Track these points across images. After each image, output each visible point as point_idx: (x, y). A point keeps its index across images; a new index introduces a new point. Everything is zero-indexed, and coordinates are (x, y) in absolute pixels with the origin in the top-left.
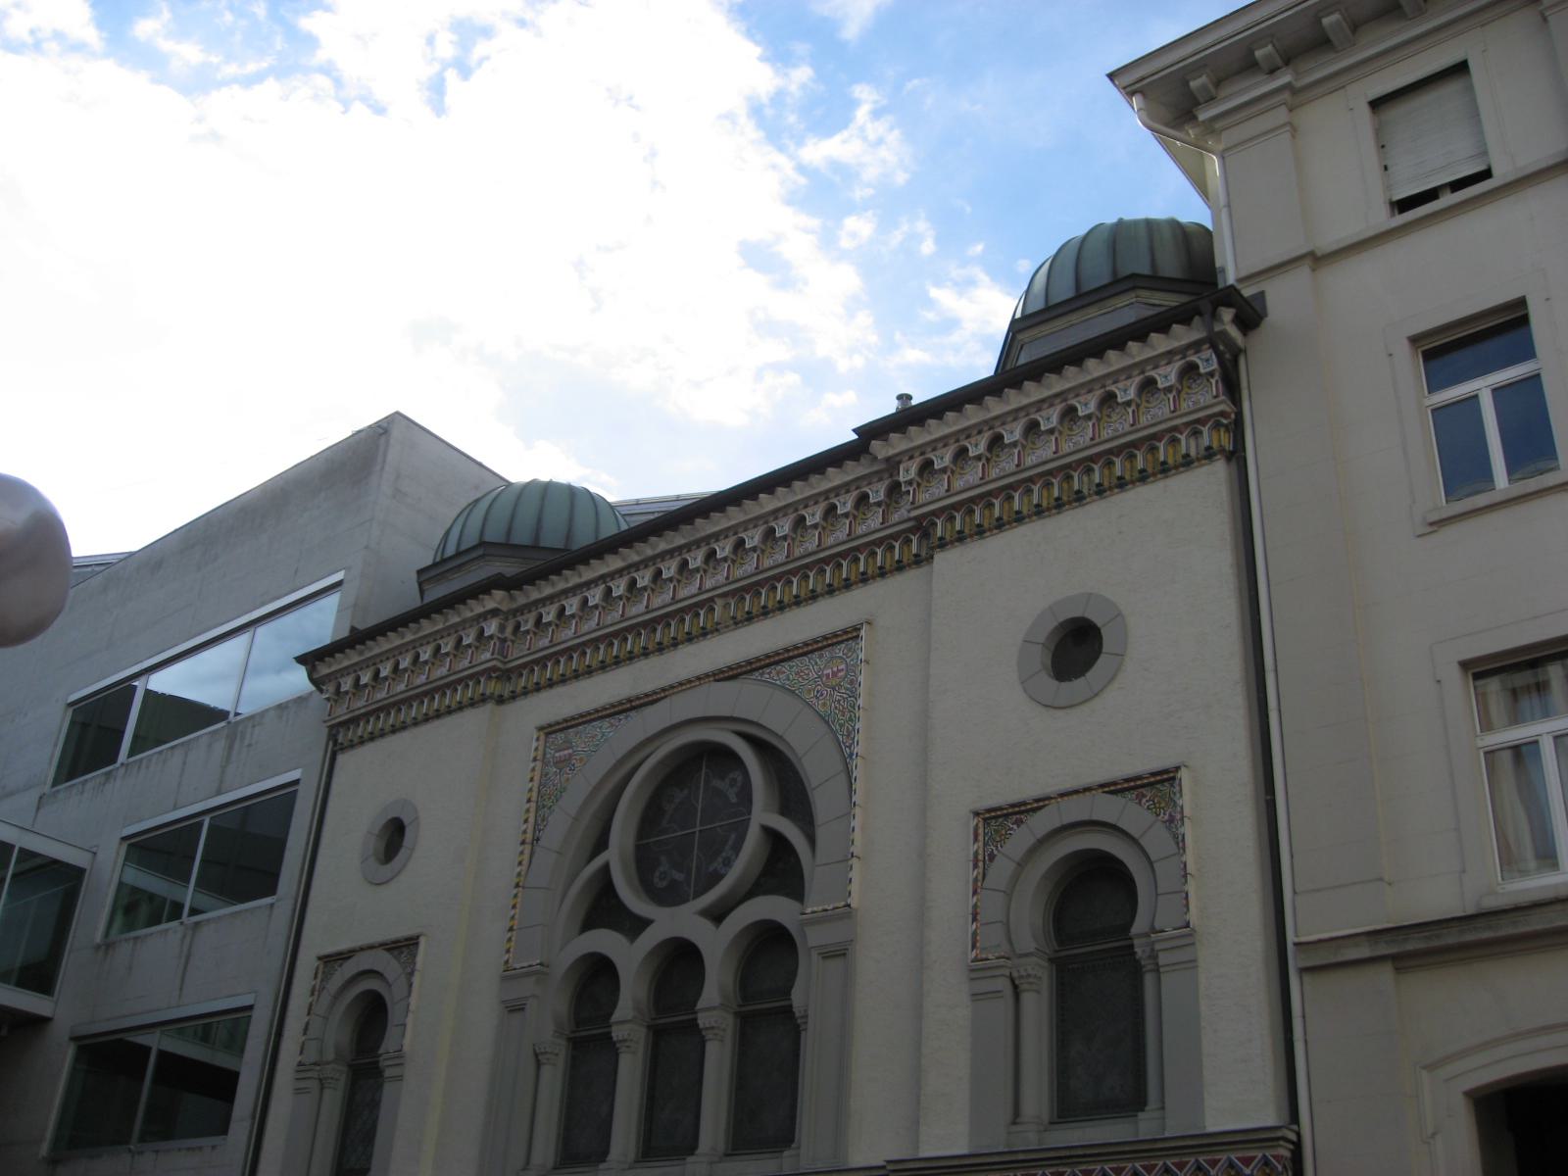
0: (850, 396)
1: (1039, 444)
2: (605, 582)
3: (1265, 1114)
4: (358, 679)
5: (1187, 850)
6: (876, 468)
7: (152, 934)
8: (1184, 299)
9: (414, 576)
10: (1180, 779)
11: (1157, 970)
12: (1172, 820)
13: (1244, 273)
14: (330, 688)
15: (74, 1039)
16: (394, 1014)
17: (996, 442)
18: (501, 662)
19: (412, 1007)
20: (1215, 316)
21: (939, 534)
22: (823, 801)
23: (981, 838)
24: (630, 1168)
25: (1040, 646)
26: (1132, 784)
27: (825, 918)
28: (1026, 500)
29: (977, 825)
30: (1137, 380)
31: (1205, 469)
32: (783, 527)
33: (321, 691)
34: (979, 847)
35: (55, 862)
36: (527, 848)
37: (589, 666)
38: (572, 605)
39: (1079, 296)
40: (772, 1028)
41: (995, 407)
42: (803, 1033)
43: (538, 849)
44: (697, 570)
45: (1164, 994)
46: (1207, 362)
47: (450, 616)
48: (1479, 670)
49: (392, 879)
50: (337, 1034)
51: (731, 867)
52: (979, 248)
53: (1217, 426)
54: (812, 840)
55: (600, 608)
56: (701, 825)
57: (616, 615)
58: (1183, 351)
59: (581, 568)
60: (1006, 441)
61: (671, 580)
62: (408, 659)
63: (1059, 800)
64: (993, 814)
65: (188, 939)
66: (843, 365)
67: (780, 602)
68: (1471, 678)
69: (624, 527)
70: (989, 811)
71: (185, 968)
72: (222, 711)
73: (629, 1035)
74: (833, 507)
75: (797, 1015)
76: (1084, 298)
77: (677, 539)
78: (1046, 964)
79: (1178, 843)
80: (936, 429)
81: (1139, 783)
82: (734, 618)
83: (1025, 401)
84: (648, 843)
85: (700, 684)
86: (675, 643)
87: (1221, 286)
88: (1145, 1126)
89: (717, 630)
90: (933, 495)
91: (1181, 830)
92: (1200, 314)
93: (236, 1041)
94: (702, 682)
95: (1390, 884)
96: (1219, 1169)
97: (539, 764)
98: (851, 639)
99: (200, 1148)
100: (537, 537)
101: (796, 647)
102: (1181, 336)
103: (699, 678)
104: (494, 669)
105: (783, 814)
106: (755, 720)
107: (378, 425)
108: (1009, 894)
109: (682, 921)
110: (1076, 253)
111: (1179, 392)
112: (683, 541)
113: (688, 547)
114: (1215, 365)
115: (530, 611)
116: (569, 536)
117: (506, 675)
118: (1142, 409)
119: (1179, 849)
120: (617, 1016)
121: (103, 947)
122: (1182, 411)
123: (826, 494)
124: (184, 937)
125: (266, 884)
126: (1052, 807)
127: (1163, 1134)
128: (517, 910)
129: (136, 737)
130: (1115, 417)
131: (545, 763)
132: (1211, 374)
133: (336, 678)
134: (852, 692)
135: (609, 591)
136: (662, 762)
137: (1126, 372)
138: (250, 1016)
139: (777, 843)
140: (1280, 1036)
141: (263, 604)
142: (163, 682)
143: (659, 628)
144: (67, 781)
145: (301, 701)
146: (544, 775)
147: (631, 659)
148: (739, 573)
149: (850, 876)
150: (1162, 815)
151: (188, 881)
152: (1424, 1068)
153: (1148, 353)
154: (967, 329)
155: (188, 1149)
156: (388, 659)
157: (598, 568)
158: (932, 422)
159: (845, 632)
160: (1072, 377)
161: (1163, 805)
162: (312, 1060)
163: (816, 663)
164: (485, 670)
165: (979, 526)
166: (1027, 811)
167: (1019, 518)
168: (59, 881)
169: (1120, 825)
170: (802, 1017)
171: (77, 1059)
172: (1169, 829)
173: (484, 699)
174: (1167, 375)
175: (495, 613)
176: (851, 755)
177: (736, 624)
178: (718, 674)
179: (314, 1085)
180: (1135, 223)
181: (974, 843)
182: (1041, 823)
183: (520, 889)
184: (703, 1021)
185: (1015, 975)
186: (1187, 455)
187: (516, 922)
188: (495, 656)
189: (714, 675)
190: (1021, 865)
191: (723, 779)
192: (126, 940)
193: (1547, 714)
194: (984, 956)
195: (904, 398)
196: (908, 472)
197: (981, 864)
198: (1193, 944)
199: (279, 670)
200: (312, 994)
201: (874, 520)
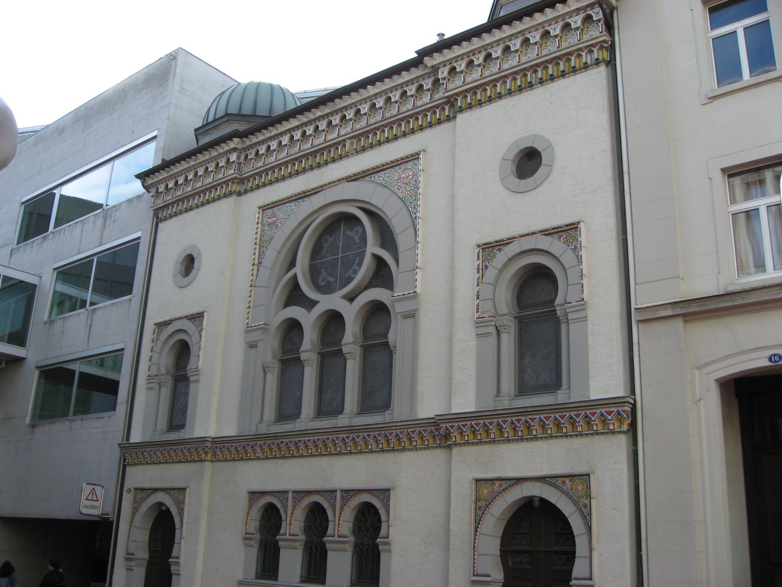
2: (290, 133)
3: (619, 391)
6: (427, 71)
22: (403, 241)
23: (481, 258)
36: (256, 267)
45: (571, 334)
85: (340, 183)
88: (561, 397)
89: (347, 156)
94: (340, 182)
103: (339, 180)
117: (242, 181)
127: (557, 402)
139: (380, 262)
159: (412, 156)
163: (398, 172)
177: (357, 152)
179: (156, 386)
197: (481, 271)
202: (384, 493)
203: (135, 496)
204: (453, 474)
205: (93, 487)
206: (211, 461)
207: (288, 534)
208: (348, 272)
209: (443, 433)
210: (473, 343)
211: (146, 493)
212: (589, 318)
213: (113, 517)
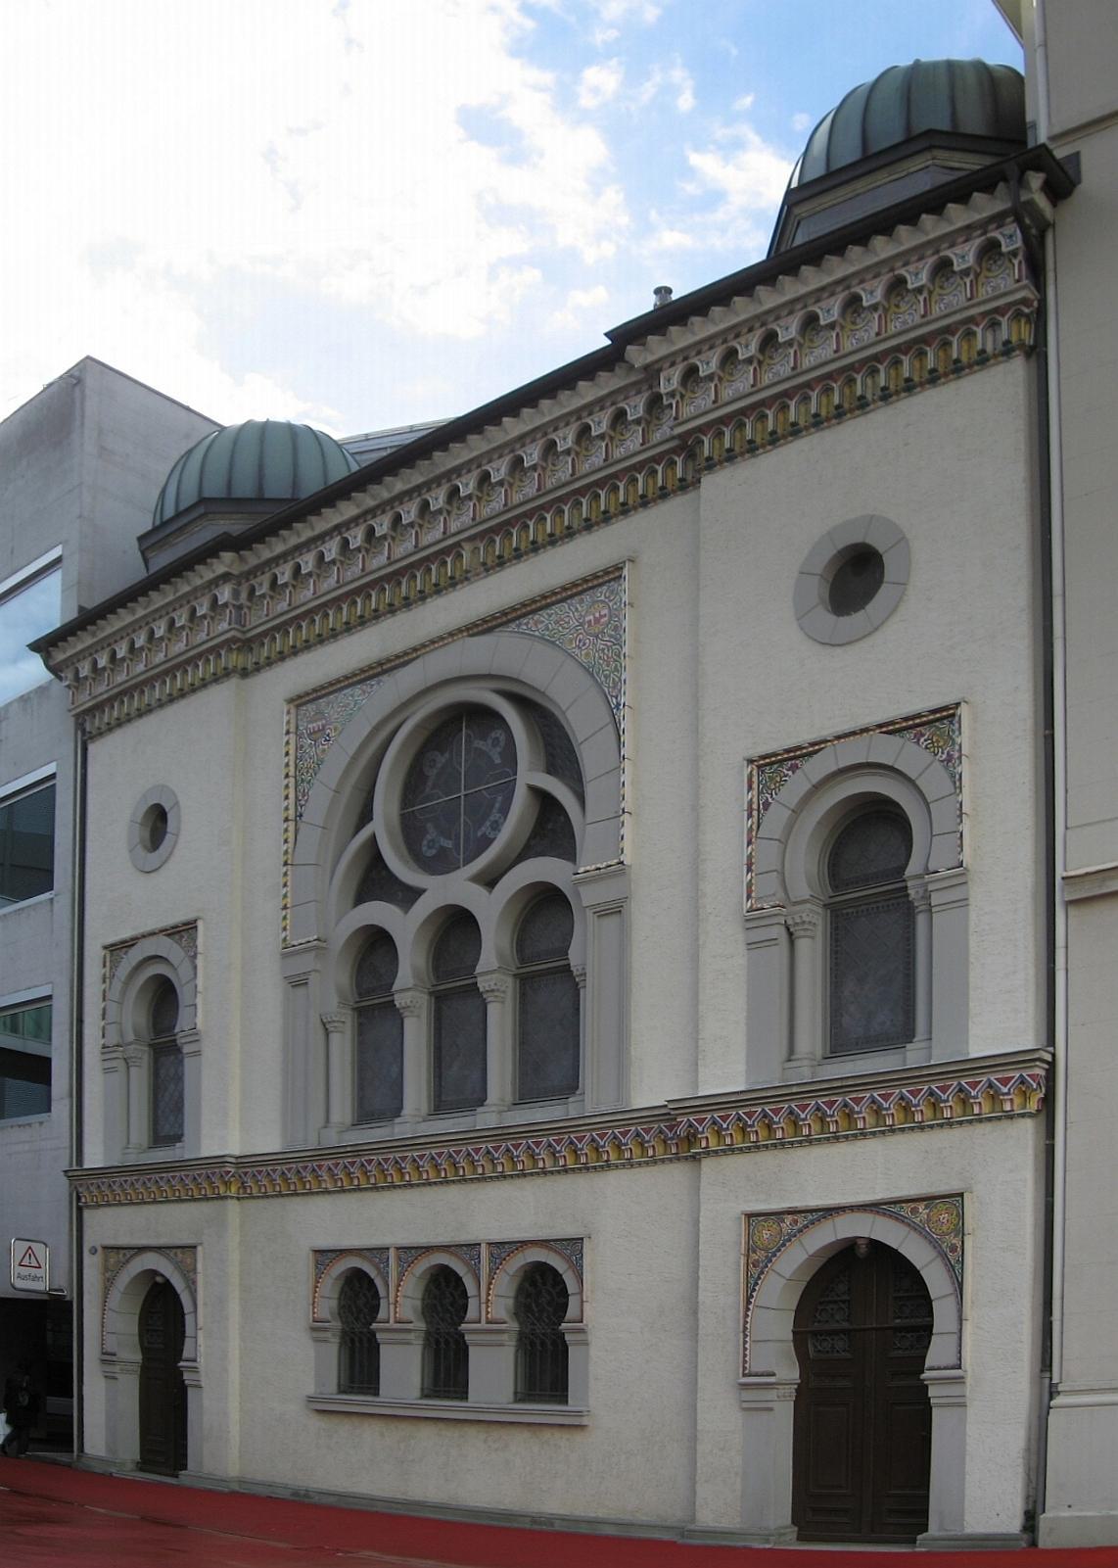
0: (600, 293)
1: (818, 341)
3: (1025, 1038)
4: (95, 662)
6: (633, 379)
8: (988, 161)
9: (135, 543)
12: (950, 758)
13: (1057, 130)
14: (69, 674)
16: (184, 995)
17: (769, 341)
20: (1021, 182)
21: (706, 453)
22: (591, 758)
27: (600, 876)
28: (803, 409)
30: (931, 261)
31: (1000, 368)
32: (532, 455)
33: (60, 678)
36: (291, 826)
38: (308, 562)
39: (866, 158)
41: (768, 298)
43: (302, 826)
44: (440, 511)
45: (936, 934)
46: (1010, 239)
50: (133, 1017)
52: (748, 100)
53: (1018, 315)
54: (581, 797)
57: (357, 570)
58: (983, 226)
59: (313, 519)
60: (781, 340)
61: (411, 525)
66: (590, 256)
67: (534, 542)
69: (355, 468)
70: (763, 757)
74: (586, 429)
76: (872, 161)
77: (413, 477)
80: (700, 329)
82: (484, 564)
83: (803, 290)
86: (423, 597)
87: (1031, 145)
88: (913, 1056)
90: (699, 406)
92: (1005, 180)
93: (43, 1030)
97: (292, 736)
100: (260, 487)
101: (554, 593)
102: (985, 206)
103: (451, 634)
104: (234, 640)
105: (549, 773)
107: (69, 374)
108: (784, 842)
110: (863, 105)
111: (977, 275)
112: (421, 480)
113: (428, 485)
114: (1019, 243)
116: (295, 484)
117: (247, 645)
118: (935, 297)
122: (981, 298)
123: (577, 413)
125: (42, 880)
126: (141, 944)
130: (904, 307)
131: (299, 736)
132: (1014, 254)
135: (346, 542)
136: (418, 727)
137: (919, 252)
139: (545, 801)
145: (42, 691)
147: (377, 618)
148: (486, 512)
153: (945, 228)
154: (733, 203)
157: (331, 517)
158: (696, 320)
159: (606, 572)
160: (857, 259)
165: (750, 442)
167: (795, 431)
172: (946, 768)
173: (227, 673)
174: (964, 255)
175: (226, 577)
179: (120, 1065)
180: (935, 65)
182: (817, 768)
186: (983, 351)
190: (796, 812)
191: (484, 738)
195: (663, 292)
196: (670, 381)
201: (633, 441)
202: (572, 1247)
203: (106, 1261)
209: (682, 1134)
212: (971, 900)
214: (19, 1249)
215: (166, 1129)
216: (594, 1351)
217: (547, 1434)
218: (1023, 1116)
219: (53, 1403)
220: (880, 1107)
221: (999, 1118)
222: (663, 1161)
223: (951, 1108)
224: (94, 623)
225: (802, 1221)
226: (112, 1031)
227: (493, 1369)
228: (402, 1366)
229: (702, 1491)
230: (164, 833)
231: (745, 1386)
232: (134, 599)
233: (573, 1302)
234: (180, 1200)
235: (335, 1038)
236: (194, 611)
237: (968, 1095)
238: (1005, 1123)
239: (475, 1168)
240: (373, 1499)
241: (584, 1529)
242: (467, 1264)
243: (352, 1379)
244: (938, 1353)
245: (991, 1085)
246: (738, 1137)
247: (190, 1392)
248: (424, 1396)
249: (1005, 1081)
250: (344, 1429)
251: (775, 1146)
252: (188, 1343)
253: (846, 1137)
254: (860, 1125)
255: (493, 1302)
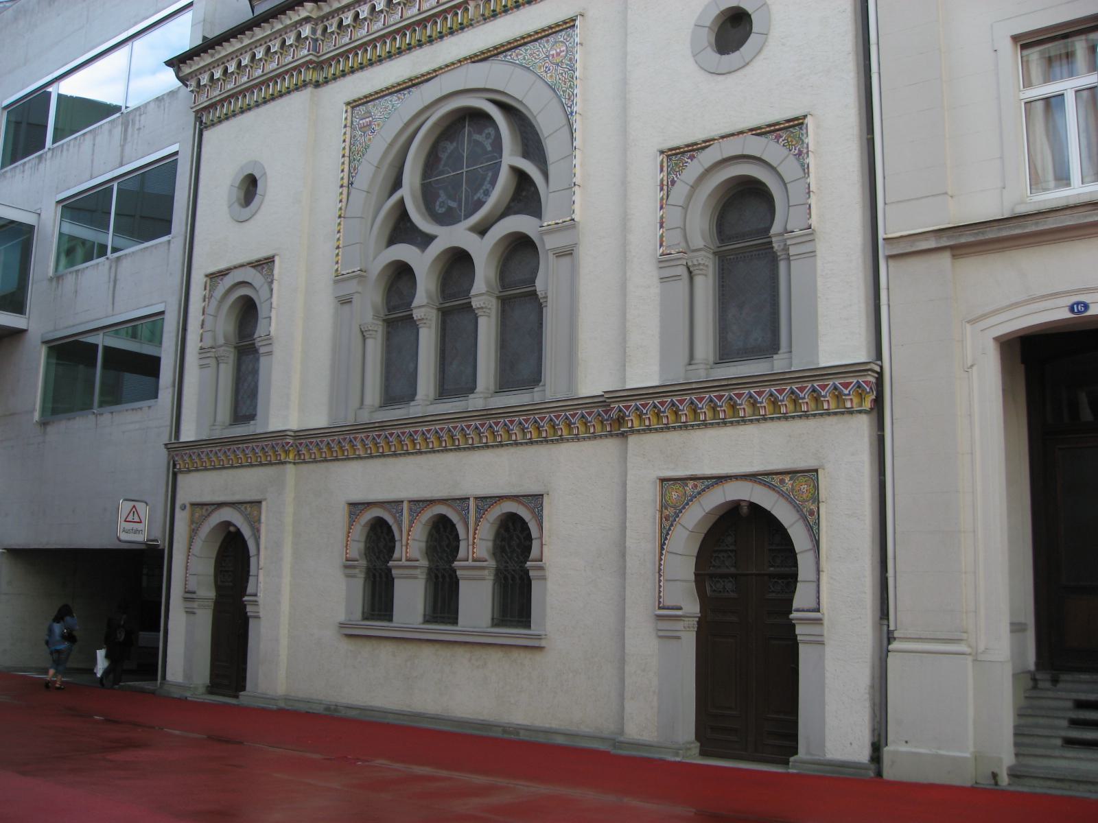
3: (859, 353)
4: (212, 75)
5: (810, 175)
7: (87, 268)
10: (807, 125)
11: (788, 259)
12: (800, 153)
15: (44, 342)
16: (262, 311)
18: (314, 55)
19: (274, 305)
22: (553, 149)
23: (665, 169)
24: (431, 404)
25: (707, 29)
26: (772, 128)
27: (558, 229)
29: (662, 160)
33: (187, 86)
34: (664, 176)
35: (12, 222)
36: (345, 190)
37: (379, 56)
40: (522, 303)
42: (544, 309)
43: (353, 191)
45: (793, 276)
47: (275, 24)
48: (1025, 42)
49: (251, 218)
50: (225, 326)
51: (489, 196)
54: (546, 175)
55: (385, 13)
56: (466, 168)
62: (247, 58)
63: (721, 140)
64: (674, 152)
65: (113, 269)
68: (1019, 47)
70: (671, 150)
71: (114, 290)
72: (116, 106)
73: (425, 315)
75: (540, 296)
78: (711, 256)
79: (804, 170)
81: (777, 127)
82: (483, 15)
84: (430, 182)
86: (441, 36)
88: (779, 364)
89: (471, 25)
91: (807, 161)
93: (156, 337)
95: (952, 197)
96: (828, 391)
97: (348, 129)
98: (569, 27)
99: (141, 409)
103: (460, 61)
104: (311, 62)
105: (524, 157)
106: (502, 89)
108: (685, 208)
109: (457, 235)
115: (333, 17)
117: (319, 66)
119: (805, 174)
120: (415, 303)
121: (55, 279)
124: (110, 268)
128: (341, 234)
129: (56, 129)
133: (196, 76)
134: (571, 67)
136: (436, 124)
138: (163, 319)
139: (522, 178)
140: (871, 302)
141: (136, 24)
142: (72, 87)
143: (429, 26)
144: (11, 164)
145: (172, 94)
146: (353, 137)
147: (409, 49)
149: (573, 198)
150: (793, 150)
151: (108, 230)
152: (968, 322)
155: (133, 410)
156: (232, 59)
159: (565, 22)
161: (794, 143)
162: (209, 345)
163: (544, 46)
164: (304, 64)
166: (698, 149)
168: (17, 236)
169: (764, 157)
170: (544, 298)
171: (49, 356)
172: (798, 160)
173: (305, 84)
175: (307, 20)
176: (572, 113)
177: (485, 19)
178: (473, 57)
179: (212, 362)
181: (660, 247)
183: (342, 219)
184: (475, 303)
185: (690, 264)
187: (341, 242)
188: (311, 52)
189: (471, 58)
191: (480, 133)
192: (70, 273)
193: (1071, 74)
194: (668, 252)
197: (665, 188)
198: (814, 240)
199: (154, 72)
200: (204, 301)
202: (535, 500)
203: (192, 515)
204: (630, 473)
205: (132, 504)
206: (294, 463)
207: (404, 559)
208: (475, 194)
209: (615, 416)
210: (655, 290)
211: (207, 510)
212: (818, 253)
213: (163, 543)
214: (125, 507)
215: (244, 410)
216: (551, 585)
217: (515, 654)
218: (860, 412)
219: (144, 637)
220: (756, 401)
221: (842, 413)
222: (601, 436)
223: (807, 404)
224: (213, 48)
225: (700, 486)
226: (208, 336)
227: (477, 598)
228: (410, 595)
229: (629, 706)
230: (255, 194)
231: (660, 618)
232: (243, 33)
233: (535, 544)
234: (252, 465)
235: (370, 342)
236: (284, 42)
237: (819, 395)
238: (847, 417)
239: (467, 439)
240: (386, 712)
241: (541, 739)
242: (460, 514)
243: (373, 608)
244: (802, 597)
245: (836, 388)
246: (654, 420)
247: (252, 623)
248: (426, 621)
249: (846, 385)
250: (366, 648)
251: (680, 427)
252: (252, 580)
253: (732, 423)
254: (742, 414)
255: (477, 544)
